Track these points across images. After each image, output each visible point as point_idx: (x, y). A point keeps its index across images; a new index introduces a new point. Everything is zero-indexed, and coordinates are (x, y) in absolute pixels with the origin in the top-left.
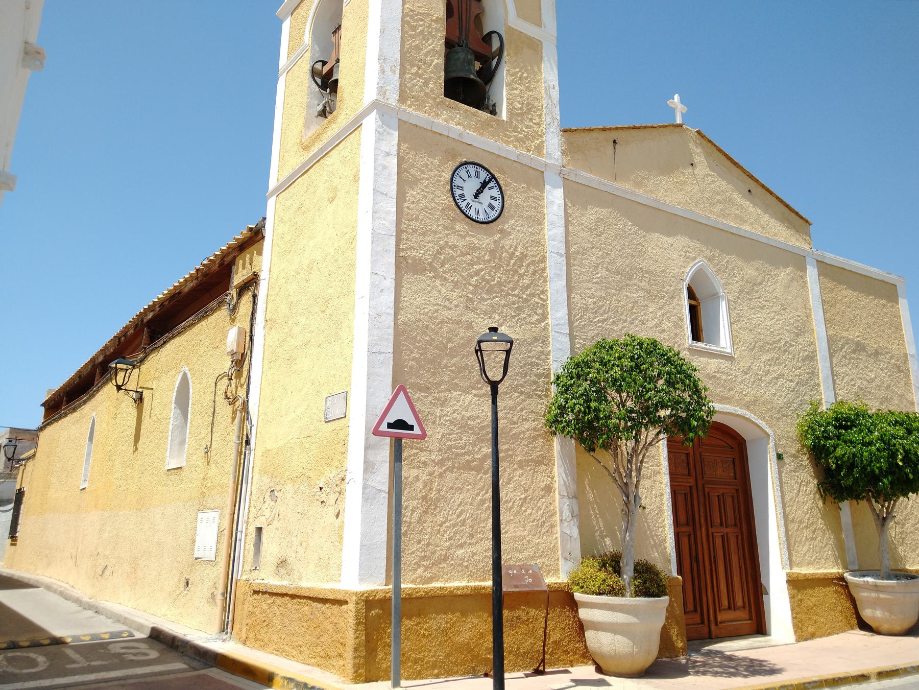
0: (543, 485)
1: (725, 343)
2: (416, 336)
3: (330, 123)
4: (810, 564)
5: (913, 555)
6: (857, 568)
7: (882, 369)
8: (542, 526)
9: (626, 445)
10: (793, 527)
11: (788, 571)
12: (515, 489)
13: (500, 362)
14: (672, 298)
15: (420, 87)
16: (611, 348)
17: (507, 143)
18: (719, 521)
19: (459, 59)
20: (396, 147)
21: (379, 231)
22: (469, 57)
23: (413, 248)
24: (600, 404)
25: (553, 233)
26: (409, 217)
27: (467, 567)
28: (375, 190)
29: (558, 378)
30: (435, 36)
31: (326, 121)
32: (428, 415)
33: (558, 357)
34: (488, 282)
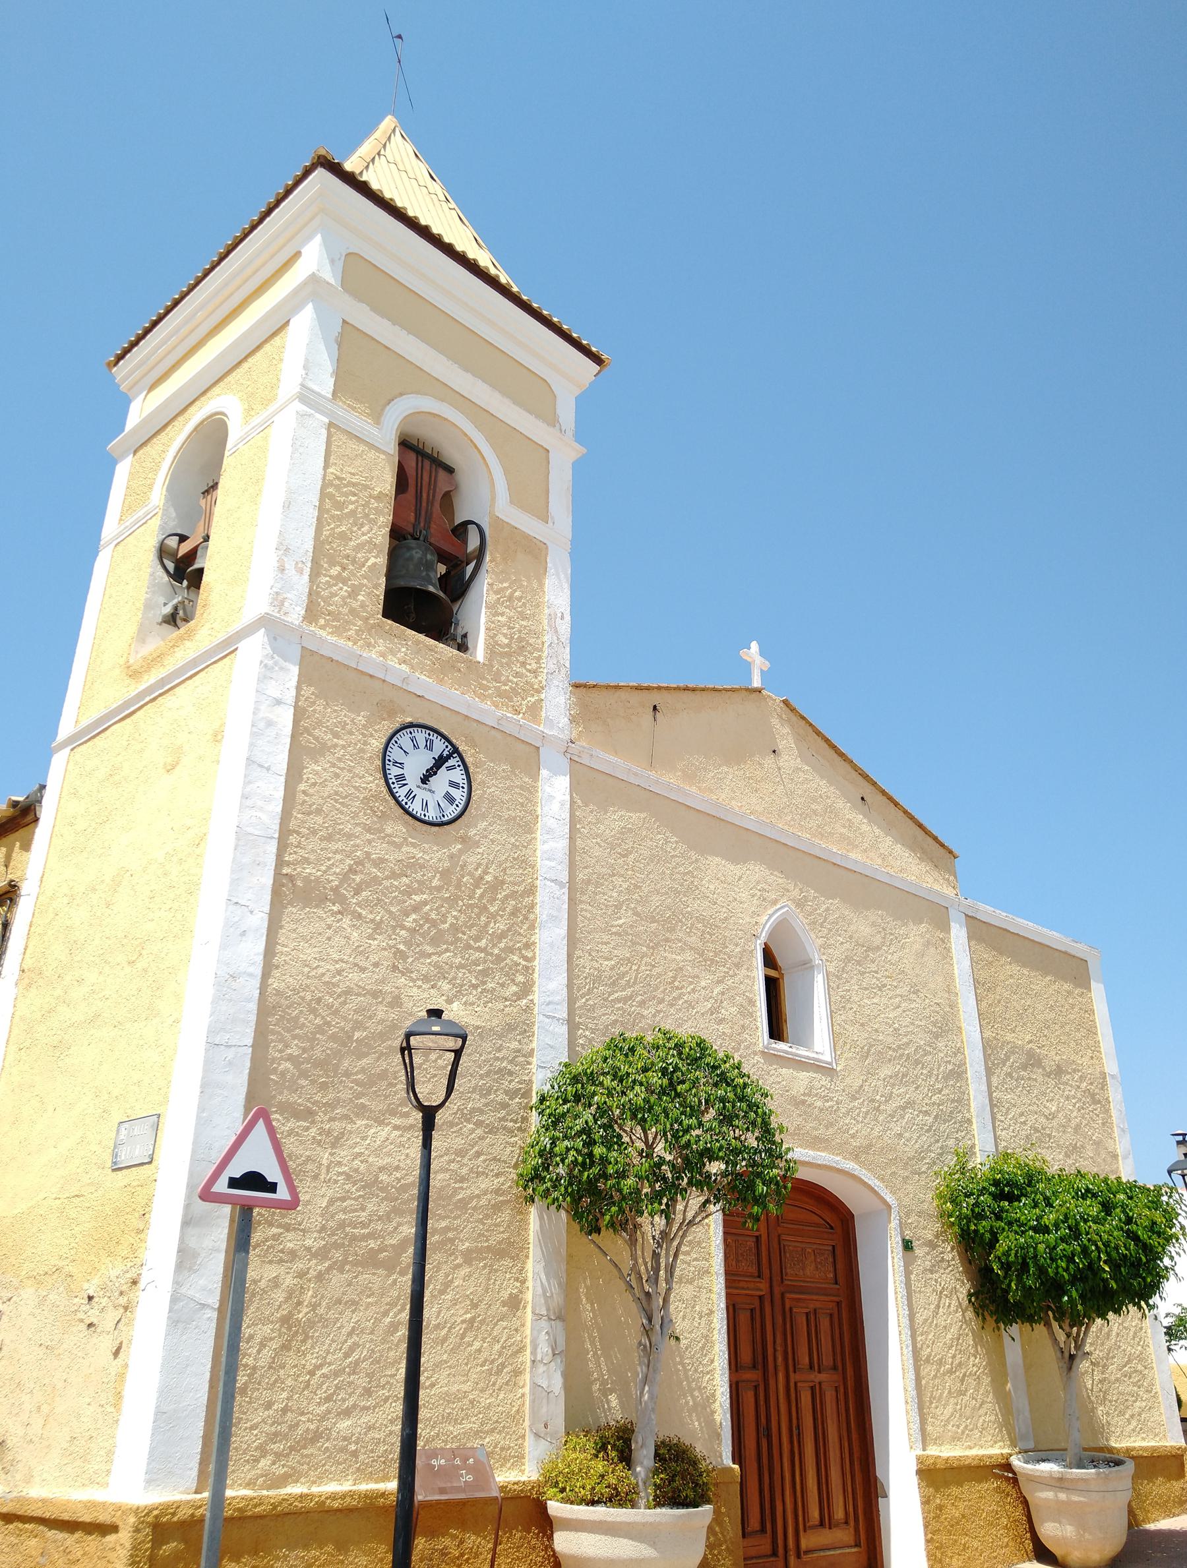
0: (505, 1295)
1: (821, 1045)
2: (297, 1017)
3: (182, 639)
4: (955, 1439)
5: (1121, 1421)
6: (1031, 1445)
7: (1068, 1098)
8: (499, 1372)
9: (651, 1225)
10: (928, 1370)
11: (920, 1452)
12: (455, 1302)
13: (444, 1068)
14: (738, 966)
15: (343, 598)
16: (632, 1050)
17: (483, 697)
18: (807, 1360)
19: (411, 558)
20: (294, 693)
21: (250, 830)
22: (429, 557)
23: (306, 861)
24: (609, 1150)
25: (550, 848)
26: (305, 808)
27: (355, 1454)
28: (250, 761)
29: (543, 1099)
30: (374, 522)
31: (176, 633)
32: (305, 1163)
33: (547, 1058)
34: (434, 924)
